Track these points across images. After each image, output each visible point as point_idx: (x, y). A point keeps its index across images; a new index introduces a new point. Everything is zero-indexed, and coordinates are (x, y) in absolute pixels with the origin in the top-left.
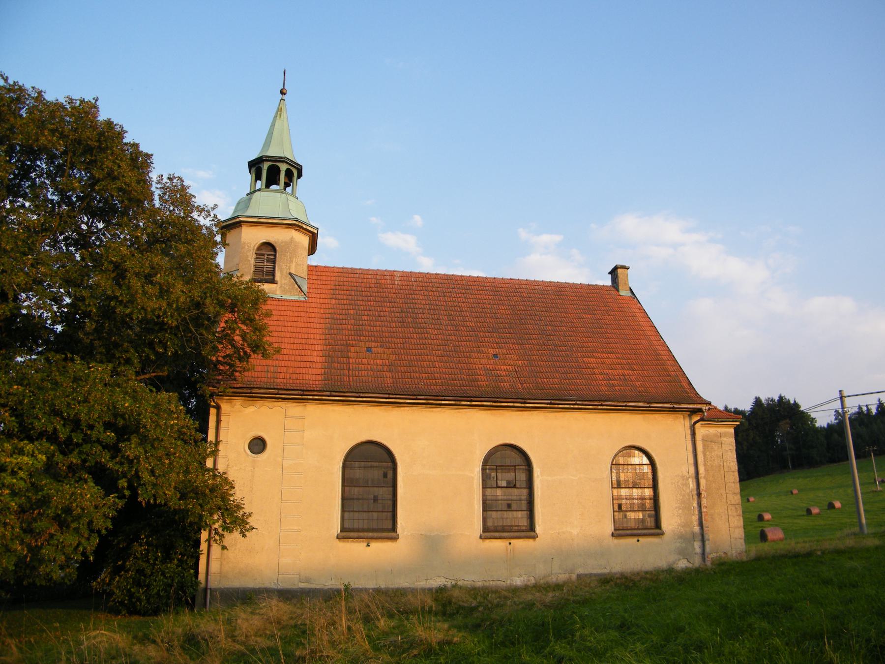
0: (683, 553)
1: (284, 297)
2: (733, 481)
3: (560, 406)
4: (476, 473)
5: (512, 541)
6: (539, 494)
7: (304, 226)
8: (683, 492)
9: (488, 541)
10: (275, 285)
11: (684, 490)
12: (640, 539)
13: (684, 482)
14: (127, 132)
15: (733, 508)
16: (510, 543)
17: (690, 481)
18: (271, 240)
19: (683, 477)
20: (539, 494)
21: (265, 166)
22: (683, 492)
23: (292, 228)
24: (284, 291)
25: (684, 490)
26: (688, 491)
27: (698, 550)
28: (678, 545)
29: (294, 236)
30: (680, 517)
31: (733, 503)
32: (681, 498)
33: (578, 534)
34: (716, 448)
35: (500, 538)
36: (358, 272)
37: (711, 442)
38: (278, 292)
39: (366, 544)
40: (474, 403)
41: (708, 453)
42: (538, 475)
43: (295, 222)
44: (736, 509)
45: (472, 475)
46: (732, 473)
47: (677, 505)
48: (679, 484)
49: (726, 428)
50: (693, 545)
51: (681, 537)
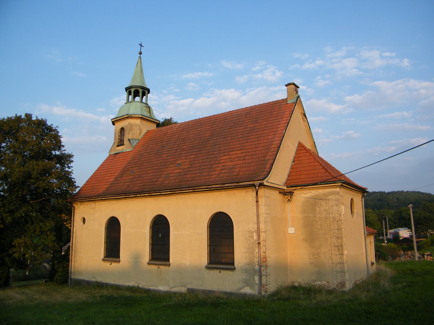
0: (247, 283)
1: (127, 151)
2: (337, 228)
3: (177, 192)
4: (147, 230)
5: (160, 266)
6: (172, 241)
7: (133, 116)
8: (249, 242)
9: (150, 266)
10: (124, 146)
11: (250, 241)
12: (222, 271)
13: (250, 235)
14: (32, 114)
15: (336, 249)
16: (159, 268)
17: (255, 234)
18: (123, 126)
19: (249, 231)
20: (172, 241)
21: (133, 90)
22: (249, 242)
23: (129, 119)
24: (127, 148)
25: (250, 241)
26: (252, 241)
27: (257, 281)
28: (244, 277)
29: (130, 122)
30: (247, 259)
31: (336, 245)
32: (248, 246)
33: (189, 265)
34: (324, 204)
35: (154, 264)
36: (225, 114)
37: (320, 199)
38: (125, 149)
39: (110, 263)
40: (142, 195)
41: (317, 208)
42: (172, 231)
43: (127, 116)
44: (339, 249)
45: (146, 232)
46: (336, 223)
47: (245, 251)
48: (247, 236)
49: (333, 188)
50: (254, 278)
51: (246, 271)
